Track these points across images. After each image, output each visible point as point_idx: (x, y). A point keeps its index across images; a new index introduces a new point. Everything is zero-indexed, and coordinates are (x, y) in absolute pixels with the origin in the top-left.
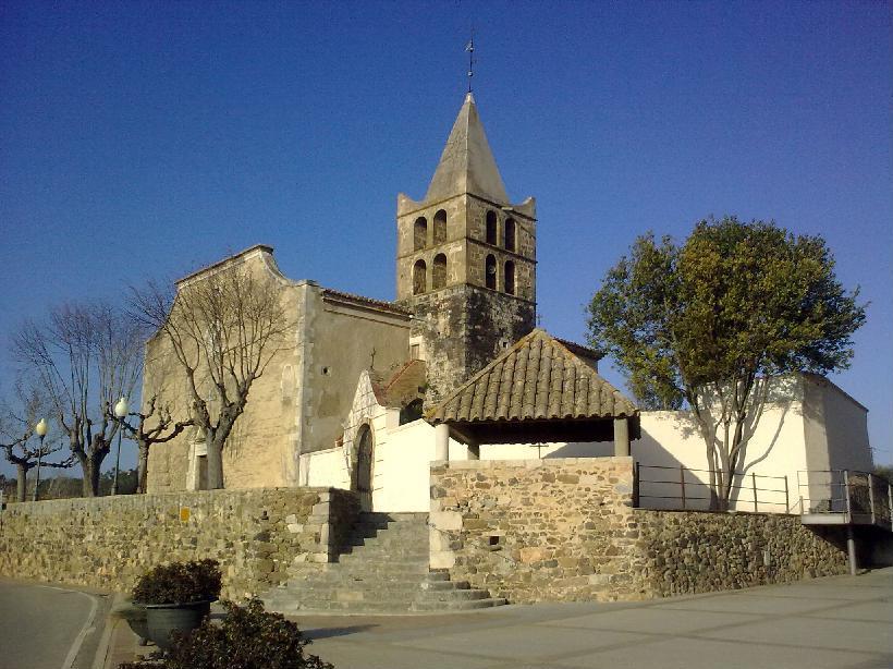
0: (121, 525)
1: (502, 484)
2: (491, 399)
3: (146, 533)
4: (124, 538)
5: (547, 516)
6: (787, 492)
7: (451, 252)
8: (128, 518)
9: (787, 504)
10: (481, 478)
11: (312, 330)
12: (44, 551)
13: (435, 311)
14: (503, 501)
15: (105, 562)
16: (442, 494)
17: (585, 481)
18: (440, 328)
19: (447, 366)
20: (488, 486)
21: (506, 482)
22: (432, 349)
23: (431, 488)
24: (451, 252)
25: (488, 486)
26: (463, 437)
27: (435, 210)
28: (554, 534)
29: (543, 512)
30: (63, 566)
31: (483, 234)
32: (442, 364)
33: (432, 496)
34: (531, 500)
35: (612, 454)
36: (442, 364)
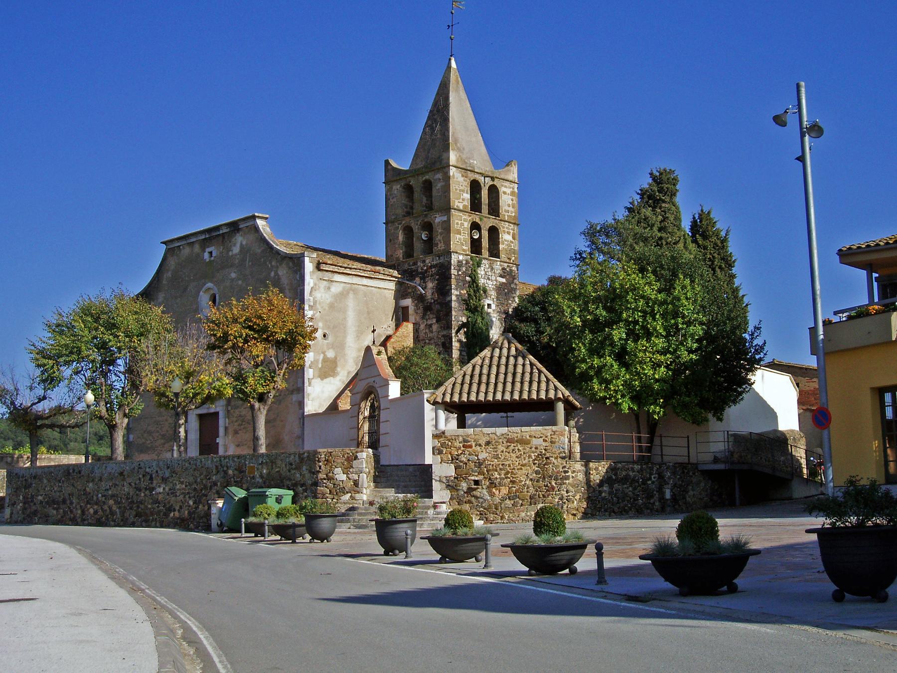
0: (191, 479)
1: (480, 445)
2: (475, 387)
3: (216, 485)
4: (195, 489)
5: (509, 466)
6: (688, 447)
7: (437, 220)
8: (197, 474)
9: (689, 456)
10: (465, 441)
11: (311, 298)
12: (111, 502)
13: (423, 277)
14: (482, 456)
15: (177, 508)
16: (440, 452)
17: (535, 442)
18: (429, 295)
19: (435, 327)
20: (471, 447)
21: (483, 443)
22: (420, 311)
23: (433, 448)
24: (437, 220)
25: (471, 447)
26: (453, 410)
27: (422, 179)
28: (515, 478)
29: (507, 463)
30: (134, 513)
31: (467, 203)
32: (431, 326)
33: (433, 454)
34: (500, 456)
35: (553, 423)
36: (431, 326)
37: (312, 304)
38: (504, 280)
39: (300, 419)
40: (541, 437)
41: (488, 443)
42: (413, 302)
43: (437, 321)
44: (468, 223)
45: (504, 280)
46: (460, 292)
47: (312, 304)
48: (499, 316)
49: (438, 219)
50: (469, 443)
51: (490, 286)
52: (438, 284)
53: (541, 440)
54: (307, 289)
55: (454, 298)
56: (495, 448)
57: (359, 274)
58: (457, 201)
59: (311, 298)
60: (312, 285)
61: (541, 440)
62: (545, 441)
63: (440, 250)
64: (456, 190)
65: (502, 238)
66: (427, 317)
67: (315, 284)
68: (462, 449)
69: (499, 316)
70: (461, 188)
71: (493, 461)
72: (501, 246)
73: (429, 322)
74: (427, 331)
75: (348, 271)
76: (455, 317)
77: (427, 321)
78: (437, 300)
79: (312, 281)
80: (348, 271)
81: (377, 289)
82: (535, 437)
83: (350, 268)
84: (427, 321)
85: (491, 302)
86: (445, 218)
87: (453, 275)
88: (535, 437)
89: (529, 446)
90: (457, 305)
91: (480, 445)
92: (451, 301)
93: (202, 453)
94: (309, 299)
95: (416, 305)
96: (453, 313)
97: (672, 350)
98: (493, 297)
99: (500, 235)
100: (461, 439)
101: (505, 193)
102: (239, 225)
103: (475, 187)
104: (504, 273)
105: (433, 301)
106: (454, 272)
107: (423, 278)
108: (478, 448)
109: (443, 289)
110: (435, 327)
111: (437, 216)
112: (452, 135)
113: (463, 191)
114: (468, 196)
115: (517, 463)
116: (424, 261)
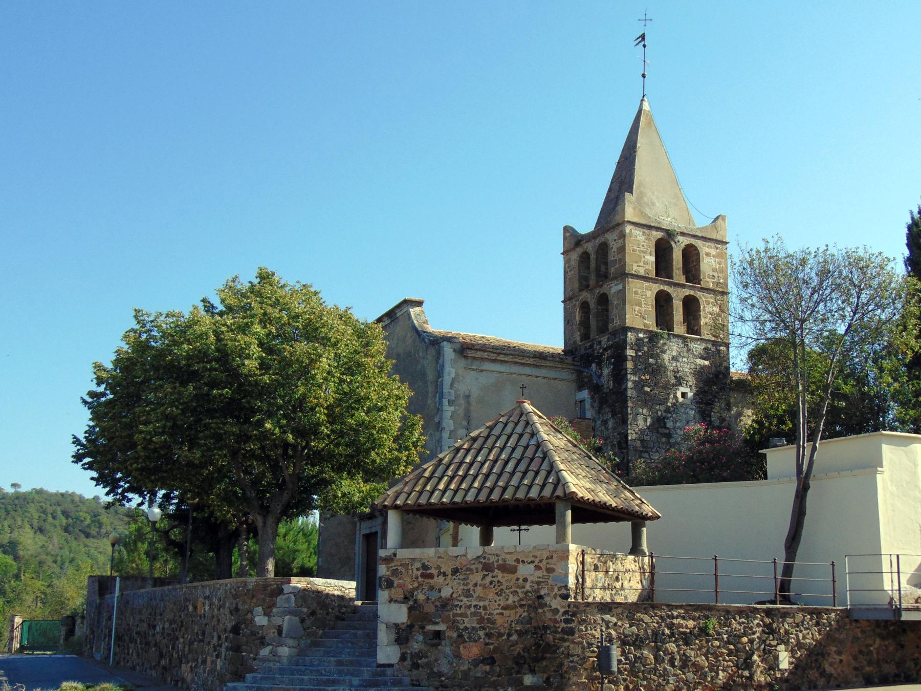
1: (444, 574)
10: (425, 567)
11: (453, 391)
14: (446, 592)
19: (611, 424)
21: (449, 572)
25: (431, 576)
27: (598, 241)
31: (652, 268)
37: (453, 398)
38: (707, 363)
39: (437, 539)
40: (533, 562)
41: (455, 571)
42: (590, 393)
43: (613, 416)
44: (652, 292)
45: (707, 363)
46: (640, 378)
47: (453, 398)
48: (699, 407)
49: (613, 288)
50: (428, 572)
51: (687, 370)
52: (614, 370)
53: (532, 566)
54: (447, 379)
55: (630, 385)
56: (464, 579)
57: (518, 361)
58: (635, 265)
59: (453, 391)
60: (453, 375)
61: (532, 566)
62: (538, 568)
63: (615, 326)
64: (634, 250)
65: (704, 310)
66: (603, 411)
67: (457, 374)
68: (420, 579)
69: (699, 407)
70: (642, 249)
71: (462, 601)
72: (703, 322)
73: (606, 417)
74: (603, 428)
75: (502, 358)
76: (631, 410)
77: (603, 415)
78: (612, 390)
79: (453, 371)
80: (502, 358)
81: (529, 378)
82: (523, 562)
83: (505, 354)
84: (603, 415)
85: (687, 390)
86: (620, 287)
87: (629, 357)
88: (523, 562)
89: (515, 576)
90: (635, 394)
91: (444, 574)
92: (626, 389)
93: (275, 576)
94: (449, 392)
95: (592, 398)
96: (630, 404)
97: (670, 405)
98: (690, 383)
99: (702, 307)
100: (418, 565)
101: (708, 255)
102: (396, 314)
103: (663, 250)
104: (708, 353)
105: (608, 391)
106: (630, 352)
107: (599, 365)
108: (441, 578)
109: (619, 375)
110: (611, 424)
111: (613, 285)
112: (637, 188)
113: (645, 252)
114: (653, 259)
115: (496, 604)
116: (600, 343)
